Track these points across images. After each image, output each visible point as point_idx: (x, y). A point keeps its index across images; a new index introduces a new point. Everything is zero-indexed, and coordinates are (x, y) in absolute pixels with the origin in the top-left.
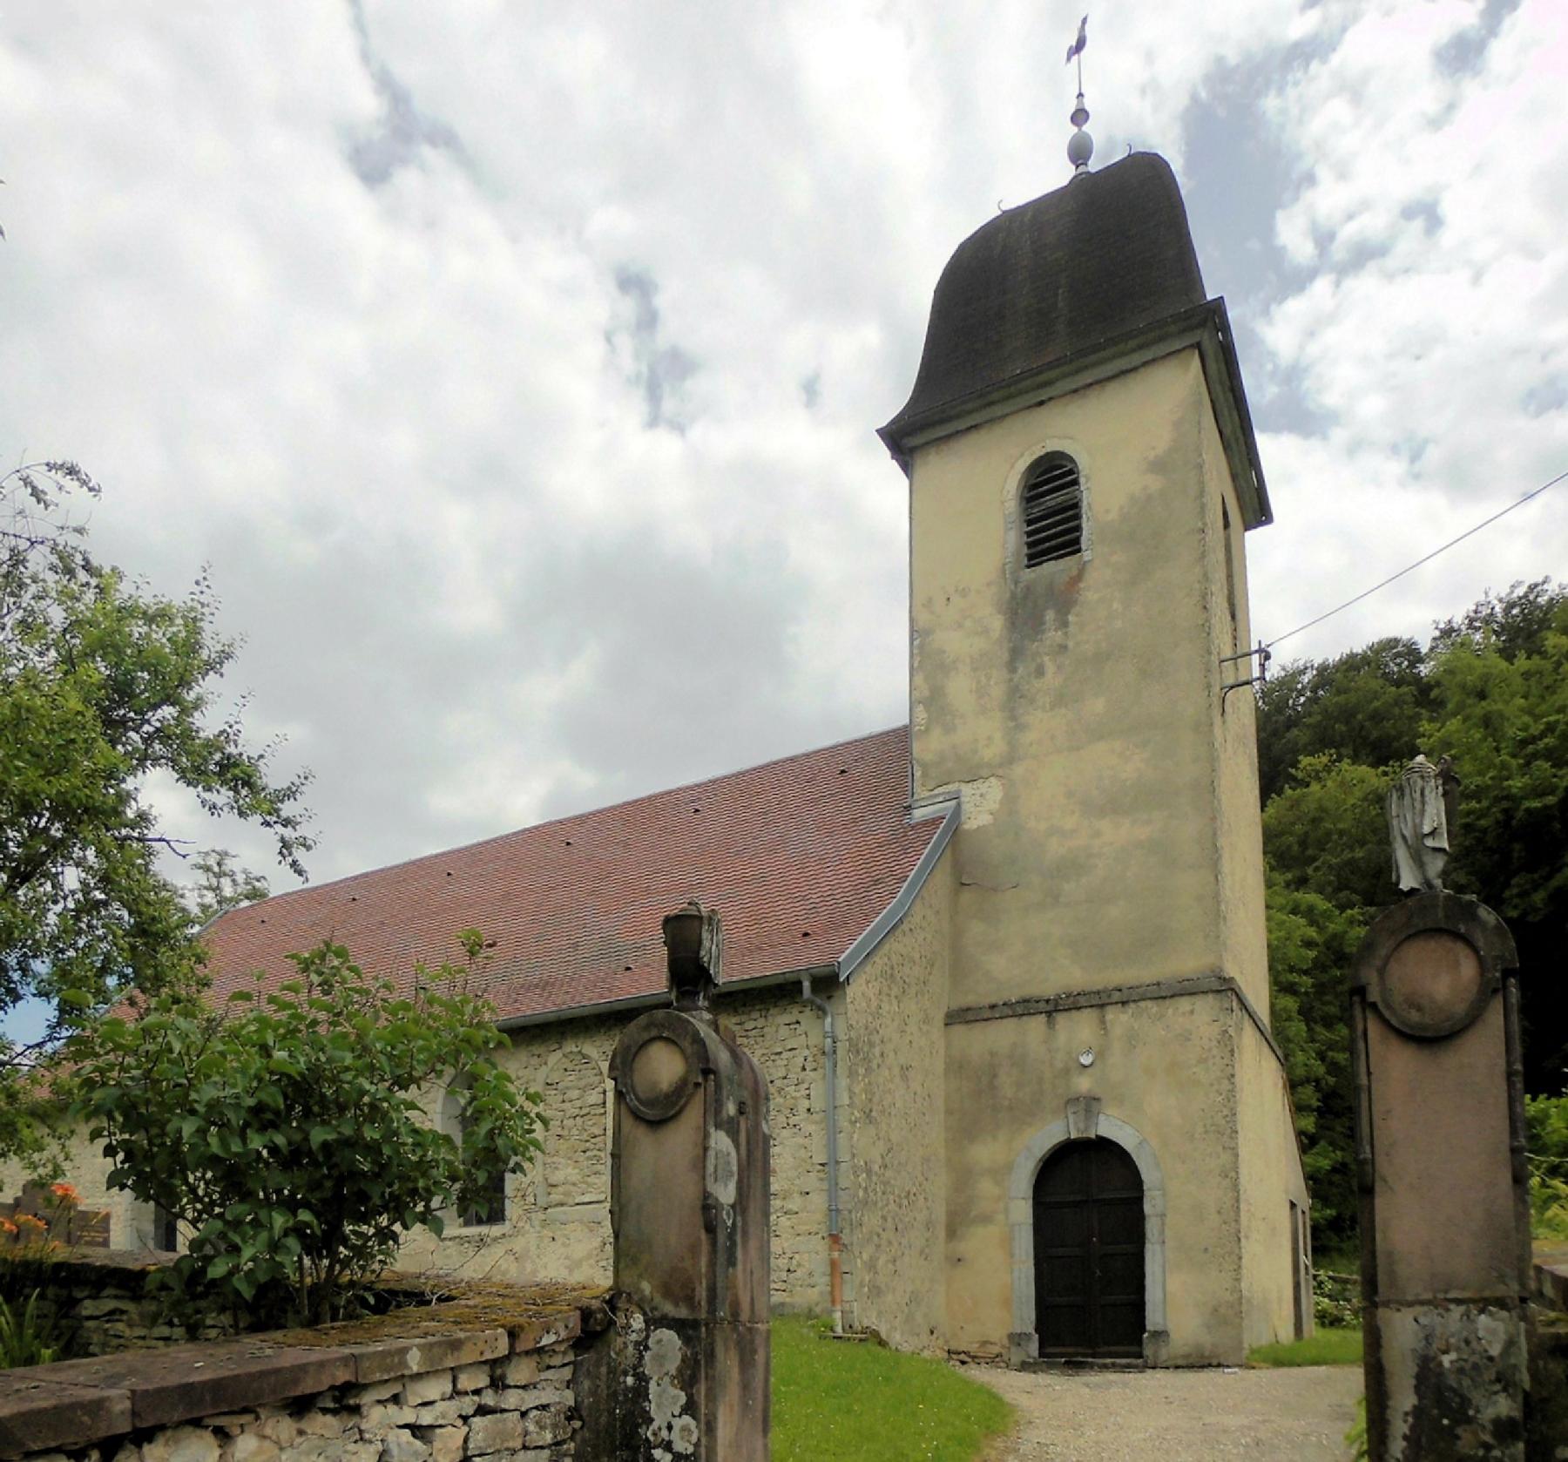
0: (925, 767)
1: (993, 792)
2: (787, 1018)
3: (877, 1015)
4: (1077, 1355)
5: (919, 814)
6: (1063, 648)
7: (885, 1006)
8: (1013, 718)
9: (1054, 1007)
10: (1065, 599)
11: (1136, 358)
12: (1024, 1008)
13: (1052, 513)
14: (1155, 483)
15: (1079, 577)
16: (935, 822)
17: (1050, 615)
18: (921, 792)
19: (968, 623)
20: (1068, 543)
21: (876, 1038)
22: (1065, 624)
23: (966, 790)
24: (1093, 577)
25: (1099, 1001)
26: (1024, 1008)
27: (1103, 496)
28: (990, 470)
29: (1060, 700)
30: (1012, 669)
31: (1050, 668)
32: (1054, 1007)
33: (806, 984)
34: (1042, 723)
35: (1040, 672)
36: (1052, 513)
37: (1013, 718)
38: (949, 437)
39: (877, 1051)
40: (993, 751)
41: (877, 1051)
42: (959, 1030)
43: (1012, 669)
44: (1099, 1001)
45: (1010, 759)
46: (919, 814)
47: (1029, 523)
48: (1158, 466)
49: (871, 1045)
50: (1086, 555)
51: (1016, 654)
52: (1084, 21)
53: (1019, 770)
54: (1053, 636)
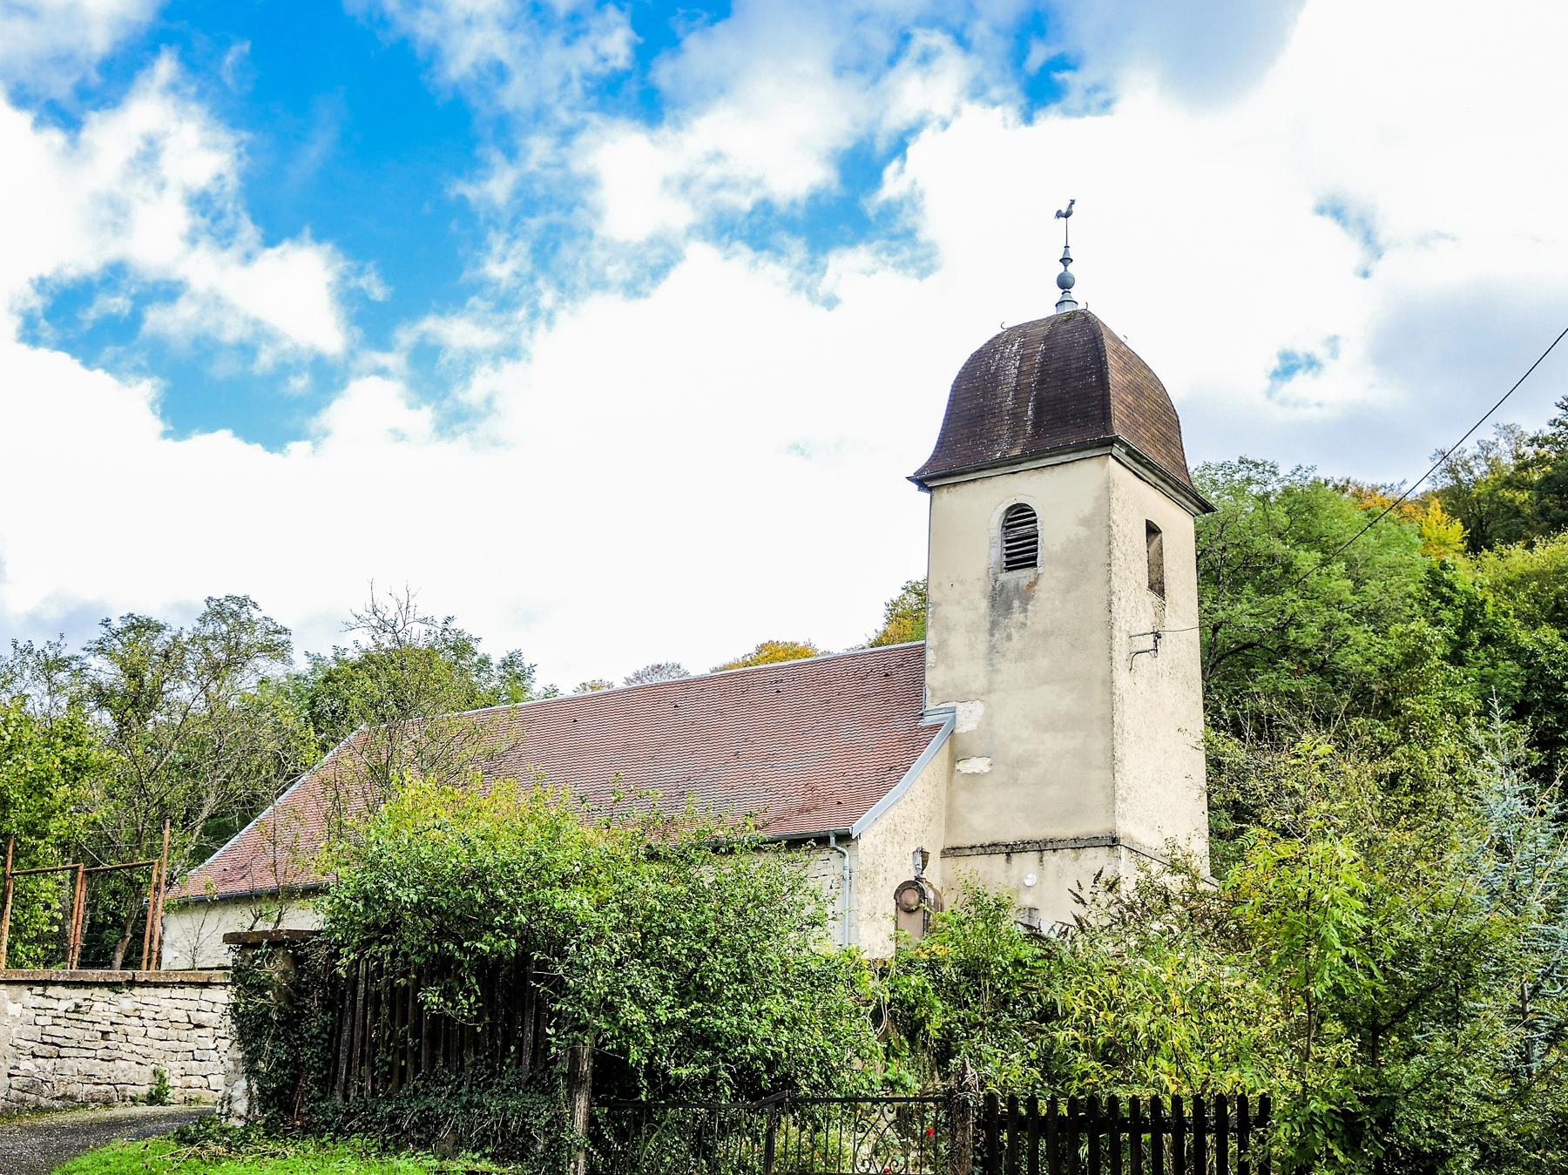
0: (933, 690)
1: (978, 709)
2: (821, 856)
3: (883, 855)
4: (151, 951)
5: (928, 721)
6: (1024, 625)
7: (889, 849)
8: (992, 665)
9: (1011, 850)
10: (1026, 595)
11: (1073, 457)
12: (991, 849)
13: (1021, 541)
14: (1083, 532)
15: (1032, 585)
16: (937, 727)
17: (1016, 603)
18: (930, 706)
19: (965, 602)
20: (1030, 561)
21: (881, 870)
22: (1025, 610)
23: (960, 707)
24: (1042, 583)
25: (1042, 847)
26: (991, 849)
27: (1052, 535)
28: (984, 502)
29: (1020, 657)
30: (992, 635)
31: (1015, 636)
32: (1011, 850)
33: (833, 839)
34: (1009, 670)
35: (1009, 638)
36: (1021, 541)
37: (992, 665)
38: (955, 484)
39: (881, 877)
40: (978, 684)
41: (881, 877)
42: (949, 861)
43: (992, 635)
44: (1042, 847)
45: (989, 691)
46: (928, 721)
47: (1008, 541)
48: (1085, 522)
49: (876, 873)
50: (1040, 570)
51: (994, 624)
52: (1073, 202)
53: (993, 698)
54: (1017, 617)
